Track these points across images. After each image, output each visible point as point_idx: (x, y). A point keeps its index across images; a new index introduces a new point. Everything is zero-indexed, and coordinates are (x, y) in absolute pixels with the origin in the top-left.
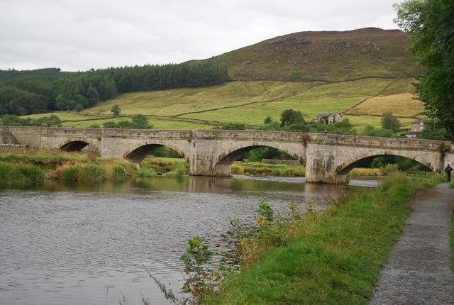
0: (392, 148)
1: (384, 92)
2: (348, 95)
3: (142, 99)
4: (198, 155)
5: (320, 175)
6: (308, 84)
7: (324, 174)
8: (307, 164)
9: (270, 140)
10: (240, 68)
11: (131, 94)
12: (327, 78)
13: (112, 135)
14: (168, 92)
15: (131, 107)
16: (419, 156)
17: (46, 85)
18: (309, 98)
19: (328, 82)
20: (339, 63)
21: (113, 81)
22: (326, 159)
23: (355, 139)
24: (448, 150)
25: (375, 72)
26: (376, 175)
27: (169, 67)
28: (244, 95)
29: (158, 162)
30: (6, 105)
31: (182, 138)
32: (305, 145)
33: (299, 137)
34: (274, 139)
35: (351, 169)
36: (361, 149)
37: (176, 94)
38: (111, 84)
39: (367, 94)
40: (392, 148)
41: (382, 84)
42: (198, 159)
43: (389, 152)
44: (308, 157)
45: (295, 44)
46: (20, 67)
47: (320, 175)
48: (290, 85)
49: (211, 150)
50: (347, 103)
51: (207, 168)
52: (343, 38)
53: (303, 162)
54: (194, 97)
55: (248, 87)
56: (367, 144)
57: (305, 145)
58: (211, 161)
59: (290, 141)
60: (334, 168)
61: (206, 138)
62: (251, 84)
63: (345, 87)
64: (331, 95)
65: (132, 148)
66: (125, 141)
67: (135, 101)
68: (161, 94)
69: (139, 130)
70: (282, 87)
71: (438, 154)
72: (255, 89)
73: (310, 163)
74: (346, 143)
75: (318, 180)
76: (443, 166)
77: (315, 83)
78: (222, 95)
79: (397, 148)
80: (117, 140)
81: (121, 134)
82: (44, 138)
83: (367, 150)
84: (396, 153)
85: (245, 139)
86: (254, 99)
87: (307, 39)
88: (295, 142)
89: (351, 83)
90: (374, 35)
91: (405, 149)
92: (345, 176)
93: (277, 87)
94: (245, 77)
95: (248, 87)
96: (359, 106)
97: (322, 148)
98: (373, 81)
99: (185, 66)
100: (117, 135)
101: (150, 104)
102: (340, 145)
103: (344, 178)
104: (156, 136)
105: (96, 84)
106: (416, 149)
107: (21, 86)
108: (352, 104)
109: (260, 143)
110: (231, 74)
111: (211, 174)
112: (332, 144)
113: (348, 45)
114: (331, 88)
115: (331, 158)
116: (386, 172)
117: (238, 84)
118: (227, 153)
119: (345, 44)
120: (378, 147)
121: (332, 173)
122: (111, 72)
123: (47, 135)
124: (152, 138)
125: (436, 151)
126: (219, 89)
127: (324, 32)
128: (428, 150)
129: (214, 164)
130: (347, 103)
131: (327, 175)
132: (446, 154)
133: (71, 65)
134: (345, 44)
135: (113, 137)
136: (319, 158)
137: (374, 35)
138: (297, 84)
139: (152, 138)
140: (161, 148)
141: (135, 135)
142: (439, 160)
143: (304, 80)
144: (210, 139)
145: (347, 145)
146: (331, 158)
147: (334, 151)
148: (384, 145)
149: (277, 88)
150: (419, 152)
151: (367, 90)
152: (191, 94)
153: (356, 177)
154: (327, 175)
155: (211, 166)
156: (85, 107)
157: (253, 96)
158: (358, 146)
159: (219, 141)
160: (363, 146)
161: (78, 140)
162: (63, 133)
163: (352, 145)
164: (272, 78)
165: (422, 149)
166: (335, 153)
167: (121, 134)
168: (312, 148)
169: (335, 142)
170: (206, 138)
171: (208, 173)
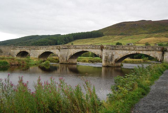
0: (139, 50)
1: (146, 37)
2: (136, 38)
3: (80, 41)
4: (61, 55)
5: (108, 63)
6: (125, 36)
7: (109, 62)
8: (103, 58)
9: (88, 49)
10: (106, 32)
11: (77, 40)
12: (130, 34)
13: (34, 48)
14: (87, 39)
15: (76, 43)
16: (152, 54)
17: (55, 38)
18: (125, 39)
19: (131, 35)
20: (134, 30)
21: (72, 37)
22: (110, 56)
23: (123, 47)
24: (166, 51)
25: (144, 32)
26: (141, 61)
27: (87, 33)
28: (107, 39)
29: (55, 58)
30: (45, 44)
31: (57, 49)
32: (102, 50)
33: (99, 47)
34: (90, 48)
35: (125, 59)
36: (126, 51)
37: (89, 39)
38: (72, 37)
39: (142, 38)
40: (139, 50)
41: (146, 35)
42: (61, 57)
43: (138, 52)
44: (103, 55)
45: (121, 25)
46: (40, 34)
47: (108, 63)
48: (120, 36)
49: (66, 53)
50: (135, 41)
51: (65, 60)
52: (135, 23)
53: (101, 57)
54: (94, 40)
55: (108, 37)
56: (128, 49)
57: (102, 50)
58: (67, 57)
59: (96, 49)
60: (114, 60)
61: (64, 49)
62: (109, 36)
63: (135, 36)
64: (131, 38)
65: (41, 53)
66: (38, 51)
67: (78, 42)
68: (85, 40)
69: (43, 46)
70: (118, 37)
71: (161, 53)
72: (110, 38)
73: (104, 58)
74: (119, 49)
75: (107, 65)
76: (164, 58)
77: (127, 35)
78: (101, 39)
79: (141, 50)
80: (36, 50)
81: (37, 48)
82: (12, 50)
83: (128, 51)
84: (141, 52)
85: (79, 48)
86: (110, 40)
87: (125, 24)
88: (98, 49)
89: (137, 35)
90: (144, 22)
91: (145, 51)
92: (120, 63)
93: (116, 37)
94: (108, 34)
95: (108, 37)
96: (139, 41)
97: (108, 51)
98: (143, 35)
99: (92, 32)
100: (36, 48)
101: (82, 42)
102: (116, 49)
103: (120, 64)
104: (48, 48)
105: (68, 38)
106: (150, 51)
107: (49, 39)
108: (137, 41)
109: (84, 50)
110: (104, 34)
111: (67, 63)
112: (113, 49)
113: (136, 25)
114: (131, 37)
115: (113, 55)
116: (144, 60)
117: (106, 36)
118: (73, 54)
119: (135, 24)
120: (133, 50)
121: (113, 62)
122: (72, 34)
123: (13, 49)
124: (47, 49)
125: (160, 51)
126: (101, 38)
127: (130, 22)
128: (156, 51)
129: (68, 59)
130: (135, 41)
131: (111, 63)
132: (165, 52)
133: (63, 33)
134: (135, 24)
135: (34, 49)
136: (107, 56)
137: (144, 22)
138: (121, 36)
139: (47, 49)
140: (87, 53)
141: (42, 48)
142: (161, 56)
143: (125, 35)
144: (66, 49)
145: (119, 50)
146: (113, 55)
147: (114, 52)
148: (136, 49)
149: (116, 37)
150: (152, 52)
151: (142, 37)
152: (93, 40)
153: (126, 62)
154: (111, 63)
155: (66, 60)
156: (65, 44)
157: (110, 39)
158: (124, 50)
159: (69, 50)
160: (126, 50)
161: (23, 51)
162: (18, 48)
163: (121, 50)
164: (115, 35)
165: (153, 51)
166: (114, 53)
167: (37, 48)
168: (104, 51)
169: (114, 48)
170: (64, 49)
171: (65, 63)
